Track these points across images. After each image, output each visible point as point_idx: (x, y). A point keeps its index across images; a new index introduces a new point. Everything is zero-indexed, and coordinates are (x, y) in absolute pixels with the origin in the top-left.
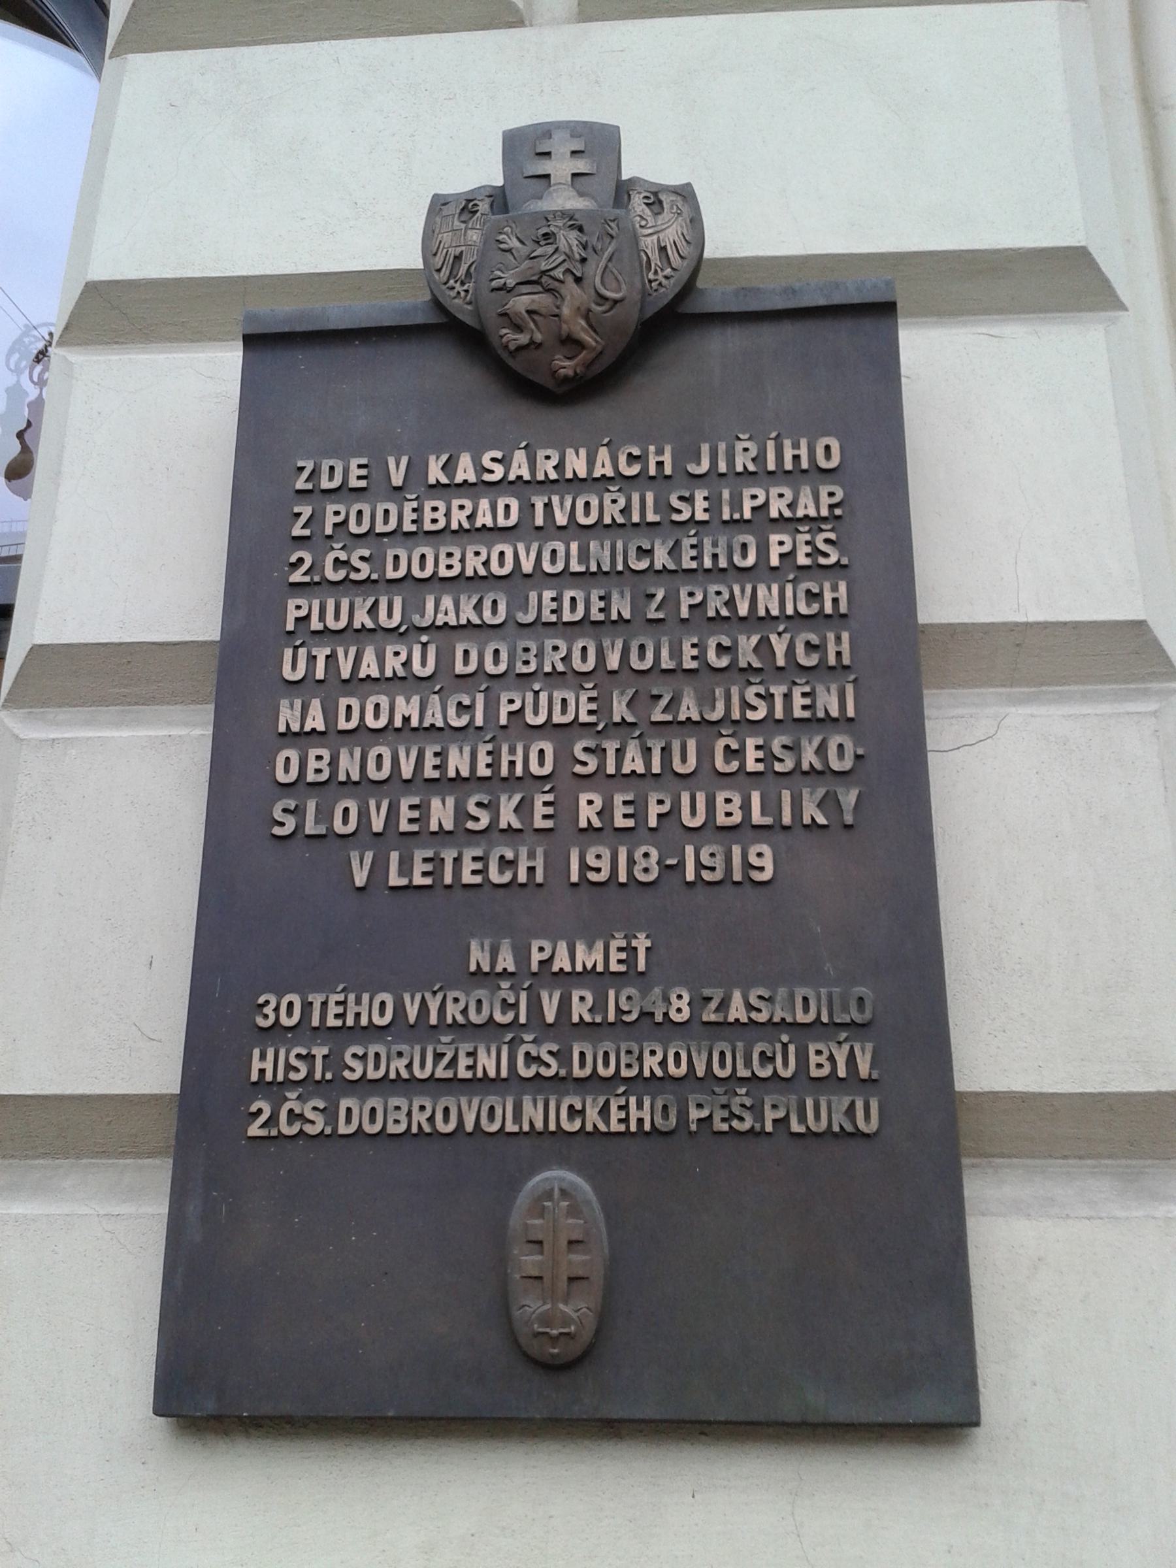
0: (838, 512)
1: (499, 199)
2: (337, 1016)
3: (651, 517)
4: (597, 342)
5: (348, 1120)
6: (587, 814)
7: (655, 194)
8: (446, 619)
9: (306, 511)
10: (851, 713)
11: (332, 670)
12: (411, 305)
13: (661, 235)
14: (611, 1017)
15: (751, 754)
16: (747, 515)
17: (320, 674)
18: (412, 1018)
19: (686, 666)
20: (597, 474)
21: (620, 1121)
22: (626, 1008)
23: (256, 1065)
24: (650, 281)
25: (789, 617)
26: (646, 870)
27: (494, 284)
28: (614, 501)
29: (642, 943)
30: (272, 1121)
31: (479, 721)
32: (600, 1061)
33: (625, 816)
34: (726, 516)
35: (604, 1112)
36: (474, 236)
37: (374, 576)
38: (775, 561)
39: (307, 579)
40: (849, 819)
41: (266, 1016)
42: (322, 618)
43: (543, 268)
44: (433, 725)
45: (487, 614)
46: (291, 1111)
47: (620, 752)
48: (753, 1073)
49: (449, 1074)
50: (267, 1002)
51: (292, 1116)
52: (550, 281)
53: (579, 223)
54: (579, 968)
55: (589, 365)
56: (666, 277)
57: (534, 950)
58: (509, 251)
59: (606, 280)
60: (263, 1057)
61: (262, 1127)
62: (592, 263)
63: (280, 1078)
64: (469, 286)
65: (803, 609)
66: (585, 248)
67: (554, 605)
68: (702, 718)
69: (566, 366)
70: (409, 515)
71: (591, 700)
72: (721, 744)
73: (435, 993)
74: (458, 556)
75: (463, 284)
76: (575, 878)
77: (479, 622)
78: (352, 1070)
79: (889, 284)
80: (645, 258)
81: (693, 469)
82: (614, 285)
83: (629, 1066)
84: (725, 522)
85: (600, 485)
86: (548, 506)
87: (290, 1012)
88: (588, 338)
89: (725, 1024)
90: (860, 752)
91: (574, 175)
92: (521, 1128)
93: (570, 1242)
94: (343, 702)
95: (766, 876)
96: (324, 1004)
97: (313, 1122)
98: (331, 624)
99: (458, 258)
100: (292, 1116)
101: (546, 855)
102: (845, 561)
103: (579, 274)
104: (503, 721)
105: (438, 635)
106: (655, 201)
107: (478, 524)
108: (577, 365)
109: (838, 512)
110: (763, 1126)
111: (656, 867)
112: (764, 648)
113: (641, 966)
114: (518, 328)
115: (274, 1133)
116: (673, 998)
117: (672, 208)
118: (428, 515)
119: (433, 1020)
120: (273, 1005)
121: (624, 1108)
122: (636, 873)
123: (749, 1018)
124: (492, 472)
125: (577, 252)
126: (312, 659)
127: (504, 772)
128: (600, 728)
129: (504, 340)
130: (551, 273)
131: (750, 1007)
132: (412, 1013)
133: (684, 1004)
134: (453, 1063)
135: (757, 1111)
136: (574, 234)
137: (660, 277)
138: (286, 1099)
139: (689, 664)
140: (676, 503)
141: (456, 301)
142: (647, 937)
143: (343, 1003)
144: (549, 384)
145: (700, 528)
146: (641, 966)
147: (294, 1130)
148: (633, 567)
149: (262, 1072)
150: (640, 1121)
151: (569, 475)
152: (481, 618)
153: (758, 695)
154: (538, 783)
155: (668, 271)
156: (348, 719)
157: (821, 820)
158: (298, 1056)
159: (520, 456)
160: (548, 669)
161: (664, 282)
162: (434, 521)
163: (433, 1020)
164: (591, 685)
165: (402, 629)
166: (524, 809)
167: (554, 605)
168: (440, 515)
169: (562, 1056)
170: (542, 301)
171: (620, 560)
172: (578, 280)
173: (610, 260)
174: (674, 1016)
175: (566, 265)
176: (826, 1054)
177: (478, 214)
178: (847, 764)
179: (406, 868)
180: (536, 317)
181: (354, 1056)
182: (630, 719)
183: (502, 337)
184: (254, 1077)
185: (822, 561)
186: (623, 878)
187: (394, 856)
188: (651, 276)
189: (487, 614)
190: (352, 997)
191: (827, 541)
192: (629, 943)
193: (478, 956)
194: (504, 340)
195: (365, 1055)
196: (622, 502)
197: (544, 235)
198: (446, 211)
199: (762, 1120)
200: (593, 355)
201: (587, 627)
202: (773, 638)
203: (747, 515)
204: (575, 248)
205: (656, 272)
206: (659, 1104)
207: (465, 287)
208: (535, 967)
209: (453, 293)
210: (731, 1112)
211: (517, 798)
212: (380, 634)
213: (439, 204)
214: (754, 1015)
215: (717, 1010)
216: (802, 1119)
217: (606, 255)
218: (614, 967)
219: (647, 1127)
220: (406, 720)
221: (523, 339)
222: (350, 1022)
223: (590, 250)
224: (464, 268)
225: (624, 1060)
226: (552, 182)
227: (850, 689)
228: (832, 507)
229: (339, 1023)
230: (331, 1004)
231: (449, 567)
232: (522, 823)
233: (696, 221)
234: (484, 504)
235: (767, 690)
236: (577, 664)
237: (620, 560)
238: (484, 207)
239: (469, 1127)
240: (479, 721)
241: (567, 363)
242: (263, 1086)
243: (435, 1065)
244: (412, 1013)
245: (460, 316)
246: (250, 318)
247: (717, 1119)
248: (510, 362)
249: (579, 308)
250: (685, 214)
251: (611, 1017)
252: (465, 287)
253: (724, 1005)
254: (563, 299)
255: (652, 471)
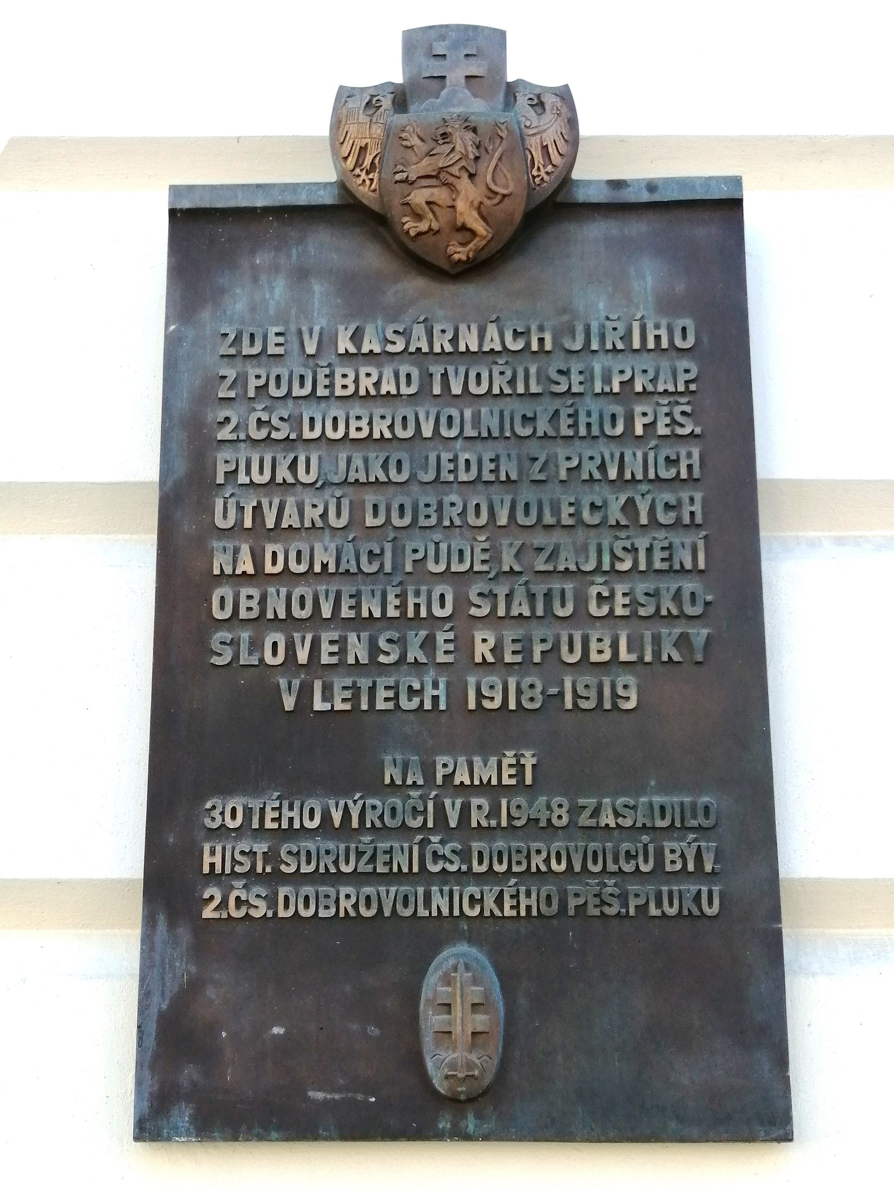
0: (693, 387)
1: (401, 98)
2: (273, 820)
3: (534, 389)
4: (487, 231)
5: (286, 906)
6: (482, 650)
7: (539, 96)
8: (357, 476)
9: (231, 374)
10: (702, 565)
11: (258, 519)
12: (327, 198)
13: (544, 135)
14: (504, 823)
15: (620, 600)
16: (616, 389)
17: (248, 523)
18: (337, 823)
19: (564, 523)
20: (486, 349)
21: (512, 907)
22: (516, 815)
23: (207, 860)
24: (534, 177)
25: (651, 481)
26: (532, 699)
27: (398, 177)
28: (502, 373)
29: (529, 761)
30: (223, 904)
31: (388, 568)
32: (495, 859)
33: (514, 652)
34: (598, 390)
35: (499, 901)
36: (377, 131)
37: (293, 436)
38: (639, 431)
39: (233, 437)
40: (699, 657)
41: (213, 819)
42: (248, 472)
43: (441, 165)
44: (348, 571)
45: (393, 472)
46: (238, 898)
47: (509, 597)
48: (620, 868)
49: (369, 868)
50: (214, 807)
51: (239, 902)
52: (448, 176)
53: (473, 125)
54: (477, 782)
55: (478, 251)
56: (547, 173)
57: (439, 767)
58: (411, 147)
59: (496, 178)
60: (213, 853)
61: (215, 909)
62: (482, 164)
63: (228, 871)
64: (375, 175)
65: (664, 474)
66: (478, 147)
67: (451, 466)
68: (578, 568)
69: (460, 253)
70: (322, 381)
71: (484, 550)
72: (594, 591)
73: (355, 802)
74: (352, 376)
75: (368, 173)
76: (472, 705)
77: (386, 480)
78: (288, 865)
79: (737, 182)
80: (530, 157)
81: (568, 344)
82: (503, 181)
83: (519, 863)
84: (597, 395)
85: (490, 358)
86: (445, 375)
87: (234, 816)
88: (479, 227)
89: (597, 827)
90: (709, 598)
91: (467, 77)
92: (430, 913)
93: (473, 1005)
94: (269, 549)
95: (631, 704)
96: (262, 810)
97: (256, 907)
98: (257, 478)
99: (363, 149)
100: (239, 902)
101: (448, 685)
102: (698, 430)
103: (472, 171)
104: (409, 568)
105: (349, 490)
106: (538, 104)
107: (383, 392)
108: (469, 252)
109: (693, 387)
110: (628, 912)
111: (540, 696)
112: (630, 506)
113: (529, 781)
114: (419, 217)
115: (225, 916)
116: (555, 807)
117: (553, 109)
118: (339, 381)
119: (355, 824)
120: (219, 810)
121: (515, 896)
122: (523, 702)
123: (617, 823)
124: (394, 343)
125: (472, 152)
126: (241, 509)
127: (411, 613)
128: (491, 576)
129: (406, 227)
130: (449, 170)
131: (617, 814)
132: (337, 817)
133: (563, 812)
134: (373, 859)
135: (624, 898)
136: (470, 135)
137: (542, 173)
138: (232, 888)
139: (567, 521)
140: (555, 376)
141: (361, 188)
142: (533, 756)
143: (279, 809)
144: (445, 266)
145: (577, 399)
146: (529, 781)
147: (241, 913)
148: (519, 433)
149: (212, 865)
150: (529, 908)
151: (462, 348)
152: (388, 476)
153: (624, 549)
154: (440, 623)
155: (550, 168)
156: (274, 563)
157: (676, 657)
158: (242, 853)
159: (419, 331)
160: (447, 523)
161: (546, 178)
162: (345, 387)
163: (355, 824)
164: (483, 538)
165: (318, 485)
166: (429, 644)
167: (451, 466)
168: (349, 381)
169: (465, 855)
170: (441, 195)
171: (507, 426)
172: (471, 176)
173: (500, 159)
174: (555, 821)
175: (463, 163)
176: (678, 853)
177: (382, 109)
178: (697, 610)
179: (327, 695)
180: (435, 208)
181: (290, 853)
182: (517, 568)
183: (404, 224)
184: (206, 869)
185: (680, 431)
186: (512, 706)
187: (318, 686)
188: (535, 173)
189: (393, 472)
190: (286, 804)
191: (683, 413)
192: (518, 761)
193: (390, 773)
194: (406, 227)
195: (298, 852)
196: (509, 374)
197: (442, 135)
198: (351, 104)
199: (627, 907)
200: (484, 242)
201: (480, 487)
202: (638, 499)
203: (616, 389)
204: (470, 149)
205: (539, 169)
206: (543, 895)
207: (371, 176)
208: (439, 781)
209: (360, 181)
210: (602, 900)
211: (423, 633)
212: (299, 488)
213: (345, 95)
214: (620, 820)
215: (591, 817)
216: (659, 904)
217: (497, 155)
218: (506, 781)
219: (534, 913)
220: (325, 566)
221: (423, 226)
222: (285, 825)
223: (482, 149)
224: (367, 163)
225: (514, 859)
226: (448, 83)
227: (701, 544)
228: (687, 382)
229: (275, 826)
230: (268, 809)
231: (359, 429)
232: (427, 659)
233: (572, 122)
234: (388, 373)
235: (633, 545)
236: (471, 520)
237: (507, 426)
238: (387, 103)
239: (387, 913)
240: (388, 568)
241: (460, 249)
242: (213, 876)
243: (357, 862)
244: (337, 817)
245: (365, 201)
246: (176, 191)
247: (590, 907)
248: (411, 246)
249: (472, 202)
250: (563, 115)
251: (504, 823)
252: (371, 176)
253: (596, 813)
254: (458, 193)
255: (535, 347)
